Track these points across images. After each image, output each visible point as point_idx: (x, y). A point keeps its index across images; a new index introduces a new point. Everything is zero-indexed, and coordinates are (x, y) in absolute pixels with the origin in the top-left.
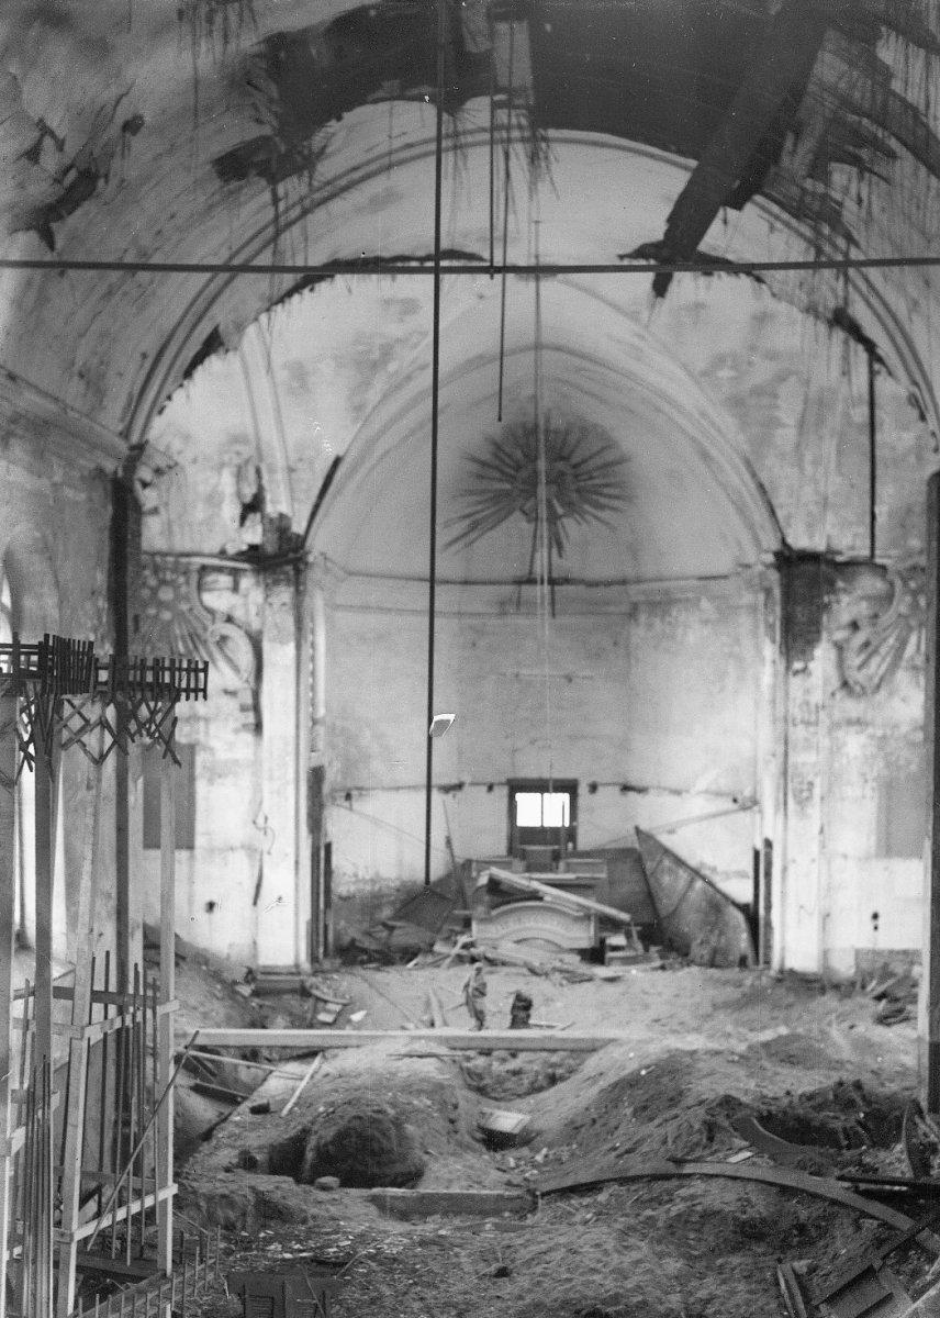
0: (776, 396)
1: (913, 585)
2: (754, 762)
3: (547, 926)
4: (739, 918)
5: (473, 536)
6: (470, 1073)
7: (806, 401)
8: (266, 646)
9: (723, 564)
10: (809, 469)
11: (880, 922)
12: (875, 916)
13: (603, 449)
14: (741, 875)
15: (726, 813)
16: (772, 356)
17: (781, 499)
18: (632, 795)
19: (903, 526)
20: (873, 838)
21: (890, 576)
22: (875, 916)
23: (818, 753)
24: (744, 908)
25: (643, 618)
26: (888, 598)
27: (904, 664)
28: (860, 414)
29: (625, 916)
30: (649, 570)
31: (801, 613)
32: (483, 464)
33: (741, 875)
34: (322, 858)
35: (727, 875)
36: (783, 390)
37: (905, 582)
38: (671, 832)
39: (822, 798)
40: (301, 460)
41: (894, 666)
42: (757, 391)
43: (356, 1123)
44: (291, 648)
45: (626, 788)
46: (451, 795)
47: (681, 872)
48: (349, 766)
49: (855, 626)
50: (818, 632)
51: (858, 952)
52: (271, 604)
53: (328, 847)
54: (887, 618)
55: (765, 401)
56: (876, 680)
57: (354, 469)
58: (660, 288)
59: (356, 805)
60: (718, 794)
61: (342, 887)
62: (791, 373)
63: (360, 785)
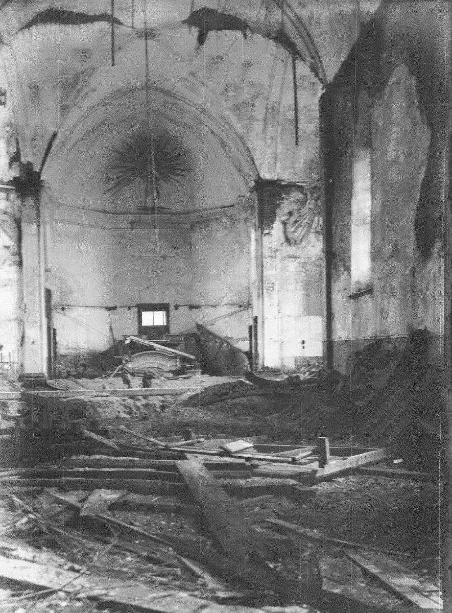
0: (253, 106)
1: (315, 195)
2: (248, 288)
3: (157, 362)
4: (245, 357)
5: (118, 188)
6: (124, 406)
7: (267, 108)
8: (23, 225)
9: (230, 199)
10: (269, 142)
11: (305, 345)
12: (303, 342)
13: (176, 148)
14: (244, 339)
15: (236, 312)
16: (251, 85)
17: (257, 155)
18: (194, 310)
19: (310, 169)
20: (301, 308)
21: (305, 191)
22: (303, 342)
23: (276, 270)
24: (246, 353)
25: (197, 229)
26: (304, 202)
27: (312, 230)
28: (291, 115)
29: (192, 357)
30: (200, 205)
31: (266, 208)
32: (122, 154)
33: (244, 339)
34: (52, 334)
35: (238, 340)
36: (257, 102)
37: (312, 193)
38: (213, 324)
39: (278, 291)
40: (37, 135)
41: (308, 231)
42: (245, 103)
43: (75, 407)
44: (34, 226)
45: (191, 307)
46: (110, 312)
47: (217, 340)
48: (63, 295)
49: (290, 214)
50: (275, 217)
51: (296, 358)
52: (25, 205)
53: (55, 330)
54: (305, 210)
55: (249, 108)
56: (300, 237)
57: (64, 143)
58: (201, 39)
59: (67, 312)
60: (233, 305)
61: (62, 350)
62: (259, 94)
63: (69, 304)
